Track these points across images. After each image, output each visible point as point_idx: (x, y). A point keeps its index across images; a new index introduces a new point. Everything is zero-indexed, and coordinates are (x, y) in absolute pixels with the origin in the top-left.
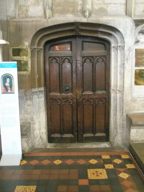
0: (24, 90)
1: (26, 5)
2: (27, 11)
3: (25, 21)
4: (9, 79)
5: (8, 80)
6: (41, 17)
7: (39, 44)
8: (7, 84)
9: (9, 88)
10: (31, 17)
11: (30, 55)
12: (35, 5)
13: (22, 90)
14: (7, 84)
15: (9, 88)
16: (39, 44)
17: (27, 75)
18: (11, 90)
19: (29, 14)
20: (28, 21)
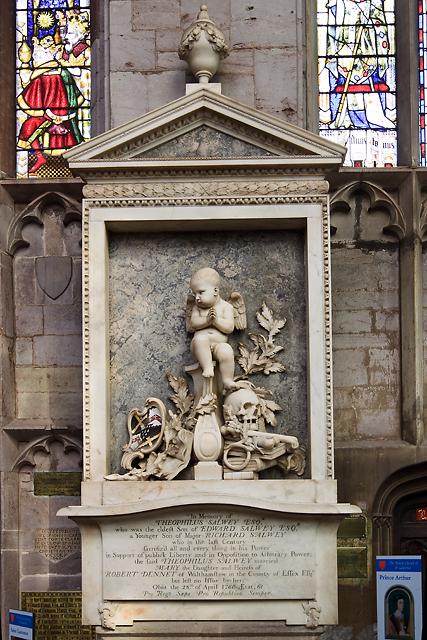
0: (350, 628)
1: (352, 408)
2: (355, 421)
3: (360, 450)
4: (402, 600)
5: (400, 603)
6: (389, 438)
7: (384, 509)
8: (398, 614)
9: (402, 625)
10: (365, 438)
11: (370, 536)
12: (376, 407)
13: (345, 629)
14: (398, 614)
15: (402, 625)
16: (384, 509)
17: (362, 587)
18: (406, 630)
19: (361, 428)
20: (366, 450)
